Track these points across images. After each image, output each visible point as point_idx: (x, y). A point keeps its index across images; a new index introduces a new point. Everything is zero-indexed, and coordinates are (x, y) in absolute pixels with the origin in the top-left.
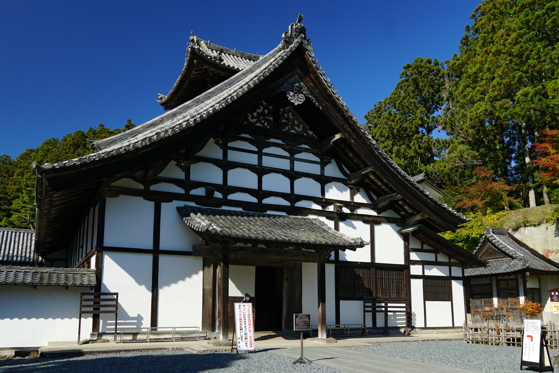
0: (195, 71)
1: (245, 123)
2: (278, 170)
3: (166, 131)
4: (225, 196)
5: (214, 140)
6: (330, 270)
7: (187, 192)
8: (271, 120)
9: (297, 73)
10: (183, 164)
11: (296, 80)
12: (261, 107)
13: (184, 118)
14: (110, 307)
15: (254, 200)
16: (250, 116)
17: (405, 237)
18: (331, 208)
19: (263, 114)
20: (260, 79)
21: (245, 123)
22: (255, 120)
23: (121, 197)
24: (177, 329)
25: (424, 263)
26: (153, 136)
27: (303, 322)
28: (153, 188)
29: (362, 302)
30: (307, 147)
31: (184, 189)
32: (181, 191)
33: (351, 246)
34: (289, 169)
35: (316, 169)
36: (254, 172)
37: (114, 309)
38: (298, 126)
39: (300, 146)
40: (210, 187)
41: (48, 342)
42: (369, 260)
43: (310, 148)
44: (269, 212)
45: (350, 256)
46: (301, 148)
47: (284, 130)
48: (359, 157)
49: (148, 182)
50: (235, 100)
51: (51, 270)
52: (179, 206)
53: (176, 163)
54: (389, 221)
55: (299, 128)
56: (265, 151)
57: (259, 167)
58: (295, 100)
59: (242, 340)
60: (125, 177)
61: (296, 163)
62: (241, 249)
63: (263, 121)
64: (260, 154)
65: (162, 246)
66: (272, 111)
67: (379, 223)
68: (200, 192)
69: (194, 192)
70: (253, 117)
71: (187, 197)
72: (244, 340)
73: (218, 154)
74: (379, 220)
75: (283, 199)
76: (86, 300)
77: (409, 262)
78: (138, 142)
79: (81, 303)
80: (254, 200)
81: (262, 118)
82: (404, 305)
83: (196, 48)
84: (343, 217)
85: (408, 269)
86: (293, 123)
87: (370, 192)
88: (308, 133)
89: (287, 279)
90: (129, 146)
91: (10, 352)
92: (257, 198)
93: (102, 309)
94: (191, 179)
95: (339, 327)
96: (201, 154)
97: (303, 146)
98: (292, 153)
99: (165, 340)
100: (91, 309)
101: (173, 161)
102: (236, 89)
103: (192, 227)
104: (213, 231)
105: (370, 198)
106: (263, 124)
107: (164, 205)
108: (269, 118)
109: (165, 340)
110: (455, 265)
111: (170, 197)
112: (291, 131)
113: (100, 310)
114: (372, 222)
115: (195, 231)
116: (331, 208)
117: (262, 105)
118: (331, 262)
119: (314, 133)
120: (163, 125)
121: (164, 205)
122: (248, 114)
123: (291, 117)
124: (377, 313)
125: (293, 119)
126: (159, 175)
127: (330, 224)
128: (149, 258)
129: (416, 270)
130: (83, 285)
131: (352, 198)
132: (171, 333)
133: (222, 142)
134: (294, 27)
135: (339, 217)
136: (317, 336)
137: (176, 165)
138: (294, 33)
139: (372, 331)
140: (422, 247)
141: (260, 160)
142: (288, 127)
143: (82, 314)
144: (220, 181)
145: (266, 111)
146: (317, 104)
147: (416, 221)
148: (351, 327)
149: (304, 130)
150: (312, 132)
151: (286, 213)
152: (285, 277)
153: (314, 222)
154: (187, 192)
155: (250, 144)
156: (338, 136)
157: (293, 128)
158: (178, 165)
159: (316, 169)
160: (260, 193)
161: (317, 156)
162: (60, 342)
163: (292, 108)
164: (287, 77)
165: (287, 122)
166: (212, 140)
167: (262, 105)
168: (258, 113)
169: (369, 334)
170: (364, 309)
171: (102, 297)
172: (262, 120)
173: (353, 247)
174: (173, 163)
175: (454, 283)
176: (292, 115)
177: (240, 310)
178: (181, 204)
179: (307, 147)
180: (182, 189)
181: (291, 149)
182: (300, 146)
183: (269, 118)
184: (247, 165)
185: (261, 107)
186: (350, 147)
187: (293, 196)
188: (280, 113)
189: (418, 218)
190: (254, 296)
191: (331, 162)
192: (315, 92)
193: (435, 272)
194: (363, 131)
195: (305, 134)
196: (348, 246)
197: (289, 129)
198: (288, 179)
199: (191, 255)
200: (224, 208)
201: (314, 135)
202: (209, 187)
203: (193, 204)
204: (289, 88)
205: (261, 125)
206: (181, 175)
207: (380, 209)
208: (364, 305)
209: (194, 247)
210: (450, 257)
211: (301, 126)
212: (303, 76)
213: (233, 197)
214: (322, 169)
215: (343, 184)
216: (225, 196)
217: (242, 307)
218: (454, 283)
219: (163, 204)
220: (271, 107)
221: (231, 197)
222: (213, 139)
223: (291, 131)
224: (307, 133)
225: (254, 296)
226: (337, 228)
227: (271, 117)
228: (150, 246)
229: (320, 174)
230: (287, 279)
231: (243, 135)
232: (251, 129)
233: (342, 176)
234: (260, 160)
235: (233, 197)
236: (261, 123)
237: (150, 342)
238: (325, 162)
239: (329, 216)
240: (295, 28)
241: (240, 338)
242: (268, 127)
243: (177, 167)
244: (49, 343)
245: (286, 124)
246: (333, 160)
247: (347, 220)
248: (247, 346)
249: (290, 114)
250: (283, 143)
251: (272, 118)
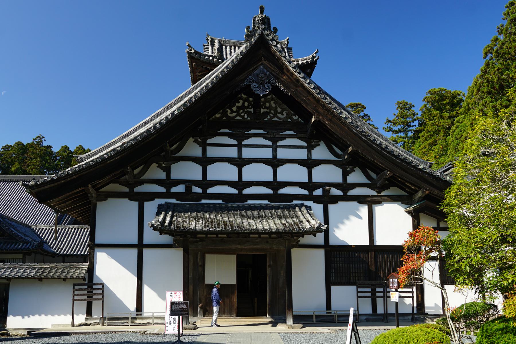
0: (199, 72)
1: (224, 118)
2: (258, 160)
4: (204, 190)
5: (193, 140)
7: (168, 190)
8: (251, 112)
9: (262, 64)
11: (261, 71)
14: (97, 295)
15: (235, 191)
16: (229, 111)
18: (319, 192)
19: (243, 107)
20: (217, 79)
21: (224, 118)
22: (234, 114)
23: (110, 200)
24: (155, 315)
27: (180, 308)
28: (137, 189)
29: (354, 288)
30: (292, 132)
32: (162, 190)
34: (272, 158)
36: (234, 165)
37: (101, 297)
38: (281, 113)
39: (284, 133)
40: (189, 183)
41: (52, 325)
42: (367, 243)
43: (295, 133)
47: (266, 119)
51: (53, 265)
52: (160, 203)
53: (157, 165)
54: (394, 199)
55: (283, 115)
56: (245, 142)
57: (238, 159)
58: (261, 91)
59: (170, 324)
61: (279, 150)
63: (242, 114)
64: (240, 146)
66: (252, 103)
67: (379, 203)
68: (180, 189)
69: (174, 190)
70: (232, 112)
72: (172, 324)
73: (197, 151)
74: (379, 199)
75: (265, 188)
76: (77, 290)
79: (74, 292)
80: (235, 191)
81: (242, 111)
82: (369, 290)
83: (193, 52)
86: (276, 111)
87: (368, 170)
88: (293, 119)
89: (270, 266)
91: (23, 332)
93: (94, 297)
95: (331, 313)
97: (287, 132)
98: (275, 141)
99: (149, 324)
100: (85, 297)
101: (154, 164)
103: (285, 211)
105: (368, 176)
106: (243, 117)
108: (249, 110)
109: (149, 324)
111: (151, 196)
112: (273, 119)
113: (93, 298)
117: (241, 98)
119: (299, 117)
122: (227, 110)
123: (274, 105)
124: (377, 299)
125: (276, 107)
126: (141, 178)
128: (134, 252)
130: (73, 277)
132: (152, 318)
133: (201, 140)
134: (257, 19)
136: (286, 323)
139: (371, 317)
140: (438, 224)
142: (270, 116)
143: (75, 302)
144: (199, 177)
145: (246, 104)
146: (285, 90)
147: (419, 197)
148: (339, 313)
149: (289, 116)
150: (297, 117)
151: (269, 201)
152: (268, 264)
154: (168, 190)
155: (229, 138)
158: (160, 167)
161: (303, 141)
162: (61, 325)
163: (274, 96)
164: (250, 70)
165: (268, 111)
166: (191, 140)
167: (241, 98)
168: (238, 107)
169: (366, 321)
170: (357, 295)
171: (94, 287)
172: (242, 113)
174: (155, 165)
176: (274, 103)
177: (171, 297)
179: (292, 132)
180: (163, 188)
181: (273, 137)
182: (284, 133)
183: (249, 110)
188: (261, 103)
189: (420, 194)
190: (235, 283)
192: (283, 79)
194: (336, 111)
195: (289, 120)
197: (272, 118)
198: (270, 167)
199: (172, 247)
201: (300, 119)
204: (254, 80)
205: (241, 118)
206: (162, 175)
208: (357, 290)
211: (284, 113)
212: (268, 65)
213: (212, 190)
214: (309, 153)
215: (334, 166)
216: (204, 190)
217: (173, 295)
219: (146, 203)
220: (251, 99)
221: (210, 191)
222: (193, 138)
223: (273, 119)
225: (235, 283)
227: (251, 108)
229: (306, 158)
230: (270, 266)
231: (222, 131)
232: (230, 124)
233: (332, 158)
234: (240, 152)
235: (212, 190)
236: (240, 116)
237: (131, 325)
238: (312, 145)
240: (258, 20)
241: (169, 323)
242: (249, 119)
243: (158, 168)
244: (52, 325)
245: (266, 114)
248: (174, 330)
250: (264, 132)
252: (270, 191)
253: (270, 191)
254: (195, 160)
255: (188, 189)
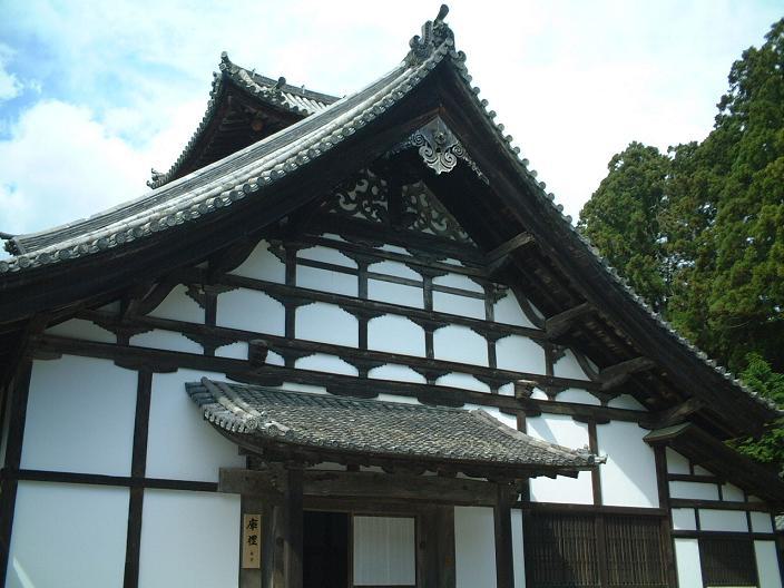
3: (173, 215)
6: (517, 520)
10: (201, 292)
12: (363, 181)
13: (210, 189)
16: (342, 199)
17: (658, 447)
18: (508, 390)
19: (368, 195)
21: (333, 211)
22: (351, 207)
25: (697, 505)
26: (143, 224)
28: (138, 340)
30: (458, 263)
31: (202, 345)
33: (568, 467)
35: (476, 309)
38: (438, 221)
40: (260, 344)
44: (383, 398)
45: (545, 490)
46: (448, 265)
47: (411, 228)
48: (566, 283)
49: (126, 325)
50: (317, 158)
53: (186, 289)
55: (441, 225)
56: (373, 268)
60: (76, 315)
62: (330, 475)
63: (368, 210)
65: (152, 472)
67: (605, 422)
68: (238, 351)
69: (224, 352)
70: (348, 200)
71: (208, 362)
73: (275, 271)
77: (668, 503)
78: (108, 236)
80: (350, 370)
81: (366, 202)
84: (535, 409)
85: (669, 518)
90: (89, 243)
92: (357, 368)
94: (218, 324)
96: (240, 272)
97: (450, 261)
102: (317, 136)
104: (272, 433)
107: (157, 379)
110: (758, 508)
111: (170, 362)
114: (591, 418)
115: (218, 427)
116: (508, 390)
118: (517, 506)
120: (163, 205)
121: (157, 379)
123: (425, 204)
127: (510, 422)
128: (122, 498)
129: (682, 520)
131: (550, 368)
135: (526, 409)
137: (187, 293)
138: (433, 38)
141: (363, 287)
142: (419, 223)
144: (279, 330)
145: (375, 190)
153: (478, 417)
156: (524, 240)
157: (427, 225)
158: (191, 293)
159: (476, 309)
160: (362, 357)
166: (263, 245)
172: (366, 206)
173: (552, 471)
175: (758, 545)
178: (195, 376)
184: (334, 297)
185: (363, 181)
186: (546, 262)
187: (433, 363)
189: (685, 409)
191: (506, 296)
193: (714, 521)
195: (453, 238)
196: (563, 467)
197: (422, 227)
200: (287, 387)
202: (256, 341)
203: (221, 378)
205: (364, 217)
206: (197, 315)
207: (605, 392)
209: (223, 472)
210: (746, 492)
211: (444, 222)
218: (758, 545)
220: (384, 183)
221: (304, 363)
224: (456, 235)
226: (522, 427)
227: (384, 201)
228: (125, 470)
231: (327, 236)
232: (343, 224)
234: (363, 287)
236: (364, 212)
239: (506, 406)
245: (414, 217)
246: (510, 292)
247: (612, 422)
249: (422, 197)
251: (385, 204)
252: (419, 379)
253: (419, 379)
254: (270, 289)
255: (257, 354)
